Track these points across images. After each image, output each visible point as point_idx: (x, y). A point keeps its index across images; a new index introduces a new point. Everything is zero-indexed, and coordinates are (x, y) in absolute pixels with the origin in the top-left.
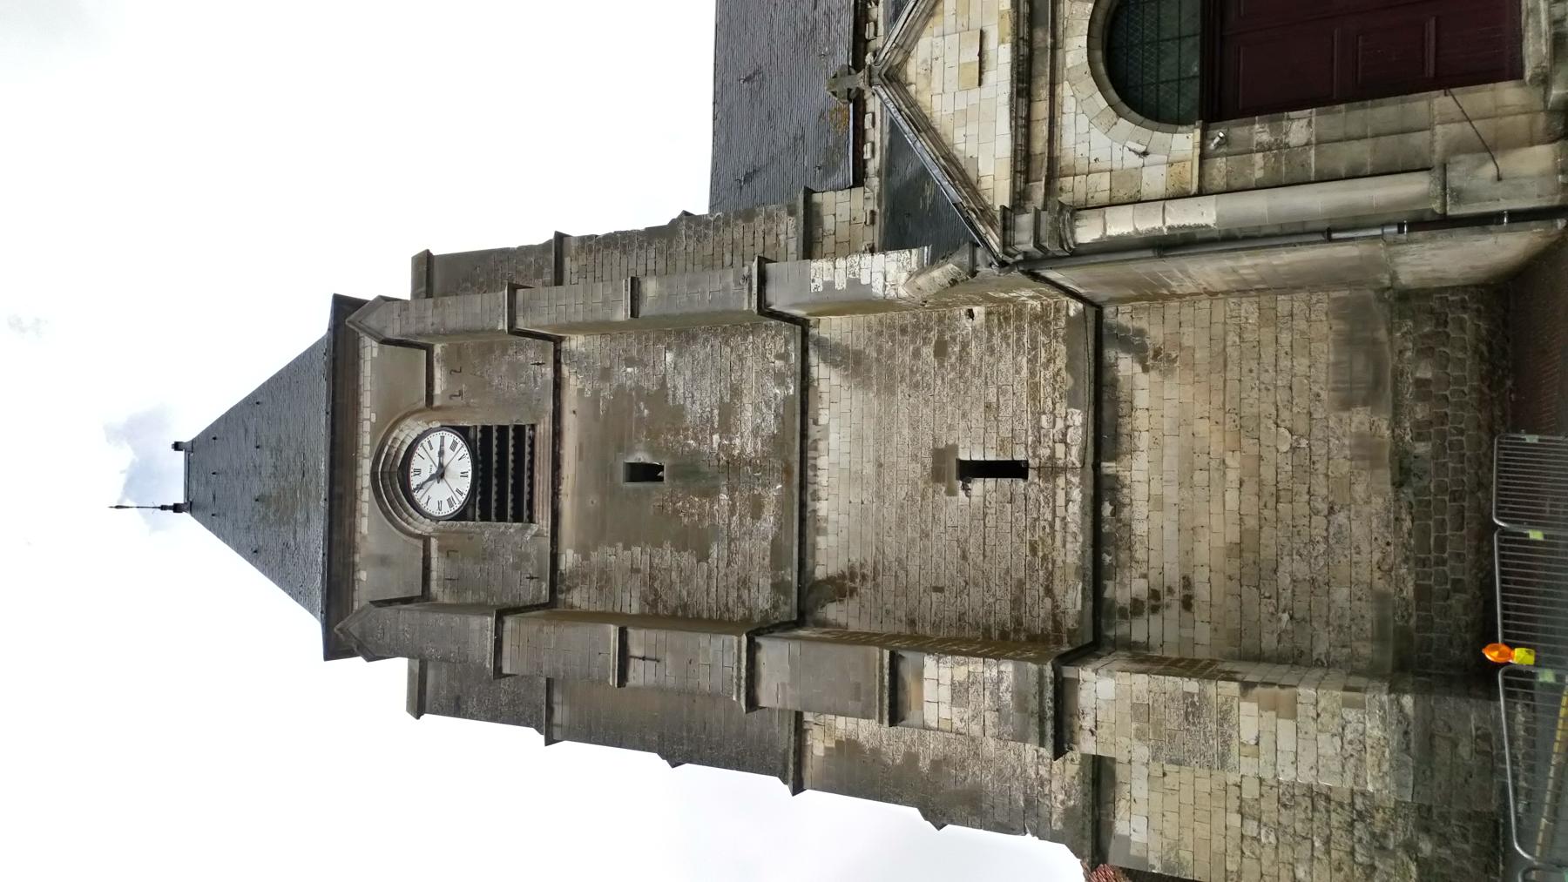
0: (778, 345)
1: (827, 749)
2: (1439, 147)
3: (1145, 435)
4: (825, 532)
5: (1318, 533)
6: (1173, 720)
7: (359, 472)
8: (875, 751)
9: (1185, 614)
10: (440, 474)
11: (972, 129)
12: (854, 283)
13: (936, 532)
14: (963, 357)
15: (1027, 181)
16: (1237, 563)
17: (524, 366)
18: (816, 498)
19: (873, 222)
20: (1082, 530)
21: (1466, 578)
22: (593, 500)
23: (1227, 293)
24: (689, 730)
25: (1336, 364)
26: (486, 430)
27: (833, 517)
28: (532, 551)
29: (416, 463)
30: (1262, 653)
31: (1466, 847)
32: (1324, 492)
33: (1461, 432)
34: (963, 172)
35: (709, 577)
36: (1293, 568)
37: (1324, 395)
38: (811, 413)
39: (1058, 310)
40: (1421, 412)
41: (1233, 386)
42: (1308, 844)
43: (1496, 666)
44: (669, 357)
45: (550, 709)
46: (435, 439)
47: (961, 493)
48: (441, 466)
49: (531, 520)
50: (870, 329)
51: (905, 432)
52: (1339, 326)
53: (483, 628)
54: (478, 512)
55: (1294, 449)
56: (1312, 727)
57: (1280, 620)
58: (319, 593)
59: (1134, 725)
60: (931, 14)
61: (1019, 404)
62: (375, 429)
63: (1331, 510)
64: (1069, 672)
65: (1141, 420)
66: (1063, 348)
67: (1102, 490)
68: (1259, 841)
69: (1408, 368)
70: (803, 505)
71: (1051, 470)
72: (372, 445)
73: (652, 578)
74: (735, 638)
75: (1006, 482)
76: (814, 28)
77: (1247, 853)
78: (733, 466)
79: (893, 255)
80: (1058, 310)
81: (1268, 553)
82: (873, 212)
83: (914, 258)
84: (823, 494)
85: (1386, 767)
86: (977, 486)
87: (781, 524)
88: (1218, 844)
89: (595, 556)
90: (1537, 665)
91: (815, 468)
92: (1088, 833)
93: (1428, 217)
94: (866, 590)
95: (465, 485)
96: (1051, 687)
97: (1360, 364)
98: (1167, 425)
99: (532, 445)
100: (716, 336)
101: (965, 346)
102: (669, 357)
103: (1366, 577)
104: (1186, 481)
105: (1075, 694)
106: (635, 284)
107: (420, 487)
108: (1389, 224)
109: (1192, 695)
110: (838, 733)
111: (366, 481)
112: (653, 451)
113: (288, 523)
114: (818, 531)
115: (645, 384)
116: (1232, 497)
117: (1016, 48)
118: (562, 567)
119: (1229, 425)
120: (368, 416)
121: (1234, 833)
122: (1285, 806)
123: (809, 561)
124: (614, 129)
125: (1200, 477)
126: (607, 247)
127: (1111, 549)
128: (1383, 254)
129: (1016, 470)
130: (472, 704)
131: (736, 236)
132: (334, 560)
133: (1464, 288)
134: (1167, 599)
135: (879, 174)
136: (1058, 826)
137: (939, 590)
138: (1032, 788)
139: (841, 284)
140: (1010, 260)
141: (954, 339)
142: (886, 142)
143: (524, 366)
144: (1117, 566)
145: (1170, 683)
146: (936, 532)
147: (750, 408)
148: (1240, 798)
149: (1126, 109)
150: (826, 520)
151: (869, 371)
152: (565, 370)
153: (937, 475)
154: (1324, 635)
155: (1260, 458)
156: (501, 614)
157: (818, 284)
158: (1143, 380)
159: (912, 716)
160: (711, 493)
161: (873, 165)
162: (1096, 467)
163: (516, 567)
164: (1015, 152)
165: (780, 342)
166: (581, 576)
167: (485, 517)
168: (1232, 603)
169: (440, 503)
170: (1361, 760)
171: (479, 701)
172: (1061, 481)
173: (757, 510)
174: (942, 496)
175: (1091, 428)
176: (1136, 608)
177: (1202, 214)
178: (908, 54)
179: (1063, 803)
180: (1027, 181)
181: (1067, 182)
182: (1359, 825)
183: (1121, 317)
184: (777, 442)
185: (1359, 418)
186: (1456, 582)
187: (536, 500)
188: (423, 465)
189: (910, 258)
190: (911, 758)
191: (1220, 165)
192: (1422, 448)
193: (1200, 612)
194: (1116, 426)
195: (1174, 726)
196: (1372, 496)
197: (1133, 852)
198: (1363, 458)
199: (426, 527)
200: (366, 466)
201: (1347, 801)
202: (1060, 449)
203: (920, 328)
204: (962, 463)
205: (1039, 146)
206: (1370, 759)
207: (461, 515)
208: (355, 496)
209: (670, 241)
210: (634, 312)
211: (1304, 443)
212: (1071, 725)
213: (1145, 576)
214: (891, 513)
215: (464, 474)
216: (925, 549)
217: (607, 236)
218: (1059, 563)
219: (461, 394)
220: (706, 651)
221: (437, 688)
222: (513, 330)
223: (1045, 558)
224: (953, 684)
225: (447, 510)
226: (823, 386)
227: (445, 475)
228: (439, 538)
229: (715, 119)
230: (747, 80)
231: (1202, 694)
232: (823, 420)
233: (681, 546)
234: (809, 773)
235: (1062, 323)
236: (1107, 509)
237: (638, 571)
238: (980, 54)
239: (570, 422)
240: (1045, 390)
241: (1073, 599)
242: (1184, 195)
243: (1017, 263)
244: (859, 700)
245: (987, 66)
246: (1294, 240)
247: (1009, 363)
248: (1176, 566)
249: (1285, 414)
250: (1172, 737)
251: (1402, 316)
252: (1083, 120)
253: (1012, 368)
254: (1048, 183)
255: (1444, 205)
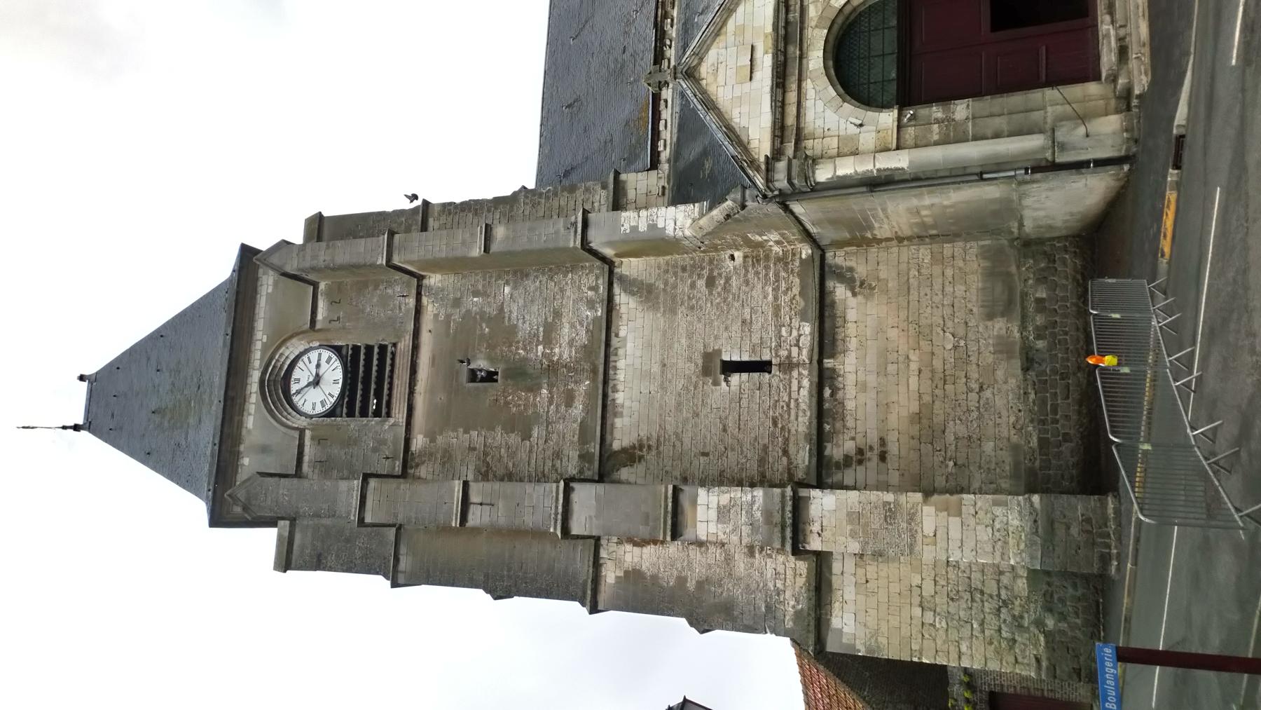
0: (590, 281)
1: (617, 577)
2: (1049, 120)
3: (854, 340)
4: (621, 415)
5: (973, 404)
6: (876, 522)
7: (249, 381)
8: (655, 578)
9: (881, 464)
10: (316, 382)
11: (745, 109)
12: (652, 227)
13: (704, 412)
14: (726, 287)
15: (782, 143)
16: (917, 427)
17: (391, 297)
18: (615, 390)
19: (663, 194)
20: (810, 407)
21: (1072, 432)
22: (441, 397)
23: (909, 239)
24: (509, 570)
25: (983, 289)
26: (356, 349)
27: (627, 404)
28: (389, 437)
29: (296, 374)
30: (940, 479)
31: (1078, 621)
32: (976, 376)
33: (1066, 333)
34: (738, 137)
35: (530, 451)
36: (956, 429)
37: (975, 310)
38: (613, 328)
39: (794, 255)
40: (1040, 320)
41: (914, 304)
42: (969, 626)
43: (1096, 366)
44: (507, 290)
45: (397, 559)
46: (314, 355)
47: (724, 384)
48: (317, 375)
49: (389, 415)
50: (659, 268)
51: (683, 341)
52: (987, 264)
53: (350, 490)
54: (345, 410)
55: (955, 347)
56: (972, 521)
57: (947, 466)
58: (205, 479)
59: (849, 527)
60: (718, 35)
61: (766, 320)
62: (265, 347)
63: (981, 388)
64: (803, 492)
65: (851, 329)
66: (797, 280)
67: (824, 379)
68: (934, 626)
69: (1031, 291)
70: (605, 396)
71: (788, 366)
72: (261, 359)
73: (486, 454)
74: (554, 485)
75: (756, 375)
76: (622, 67)
77: (927, 636)
78: (552, 368)
79: (682, 207)
80: (794, 255)
81: (939, 419)
82: (664, 188)
83: (697, 209)
84: (620, 387)
85: (1022, 546)
86: (735, 378)
87: (588, 410)
88: (905, 631)
89: (440, 440)
90: (1119, 364)
91: (615, 368)
92: (812, 628)
93: (1043, 164)
94: (651, 457)
95: (336, 390)
96: (790, 503)
97: (999, 288)
98: (869, 333)
99: (393, 359)
100: (543, 274)
101: (728, 280)
102: (507, 290)
103: (1005, 434)
104: (882, 371)
105: (807, 508)
106: (488, 229)
107: (298, 392)
108: (1020, 169)
109: (889, 504)
110: (626, 565)
111: (254, 387)
112: (491, 359)
113: (181, 427)
114: (615, 415)
115: (487, 309)
116: (913, 381)
117: (775, 56)
118: (413, 448)
119: (912, 332)
120: (261, 336)
121: (917, 622)
122: (952, 599)
123: (608, 437)
124: (471, 128)
125: (892, 368)
126: (463, 210)
127: (830, 420)
128: (1015, 197)
129: (762, 367)
130: (331, 559)
131: (562, 203)
132: (223, 448)
133: (1066, 237)
134: (869, 454)
135: (669, 161)
136: (789, 624)
137: (705, 454)
138: (771, 597)
139: (643, 227)
140: (770, 194)
141: (720, 275)
142: (675, 139)
143: (391, 297)
144: (834, 432)
145: (874, 496)
146: (704, 412)
147: (567, 326)
148: (921, 595)
149: (848, 98)
150: (623, 406)
151: (657, 298)
152: (425, 300)
153: (706, 371)
154: (977, 476)
155: (933, 354)
156: (366, 477)
157: (626, 227)
158: (852, 302)
159: (688, 534)
160: (534, 389)
161: (665, 155)
162: (820, 362)
163: (375, 450)
164: (774, 123)
165: (592, 278)
166: (428, 454)
167: (351, 414)
168: (914, 456)
169: (314, 404)
170: (1006, 543)
171: (337, 556)
172: (795, 374)
173: (569, 400)
174: (709, 387)
175: (817, 335)
176: (847, 461)
177: (900, 161)
178: (701, 59)
179: (793, 607)
180: (782, 143)
181: (809, 143)
182: (1004, 610)
183: (837, 258)
184: (587, 350)
185: (999, 325)
186: (1065, 434)
187: (394, 400)
188: (302, 375)
189: (693, 209)
190: (682, 581)
191: (910, 132)
192: (1040, 344)
193: (892, 462)
194: (834, 334)
195: (877, 526)
196: (1009, 377)
197: (844, 641)
198: (1001, 352)
199: (302, 422)
200: (255, 376)
201: (995, 593)
202: (795, 351)
203: (695, 268)
204: (724, 363)
205: (790, 120)
206: (1011, 541)
207: (331, 413)
208: (244, 400)
209: (512, 207)
210: (487, 250)
211: (962, 343)
212: (804, 530)
213: (853, 439)
214: (671, 401)
215: (336, 382)
216: (696, 425)
217: (462, 203)
218: (793, 431)
219: (339, 319)
220: (531, 496)
221: (303, 547)
222: (390, 265)
223: (783, 428)
224: (719, 507)
225: (319, 409)
226: (623, 309)
227: (319, 382)
228: (312, 430)
229: (541, 136)
230: (569, 106)
231: (896, 503)
232: (622, 334)
233: (510, 428)
234: (603, 598)
235: (797, 263)
236: (827, 392)
237: (474, 449)
238: (751, 60)
239: (426, 339)
240: (785, 310)
241: (803, 457)
242: (887, 150)
243: (775, 197)
244: (647, 524)
245: (756, 68)
246: (959, 179)
247: (760, 291)
248: (875, 432)
249: (949, 324)
250: (876, 534)
251: (1025, 257)
252: (820, 104)
253: (761, 295)
254: (796, 143)
255: (1054, 153)
